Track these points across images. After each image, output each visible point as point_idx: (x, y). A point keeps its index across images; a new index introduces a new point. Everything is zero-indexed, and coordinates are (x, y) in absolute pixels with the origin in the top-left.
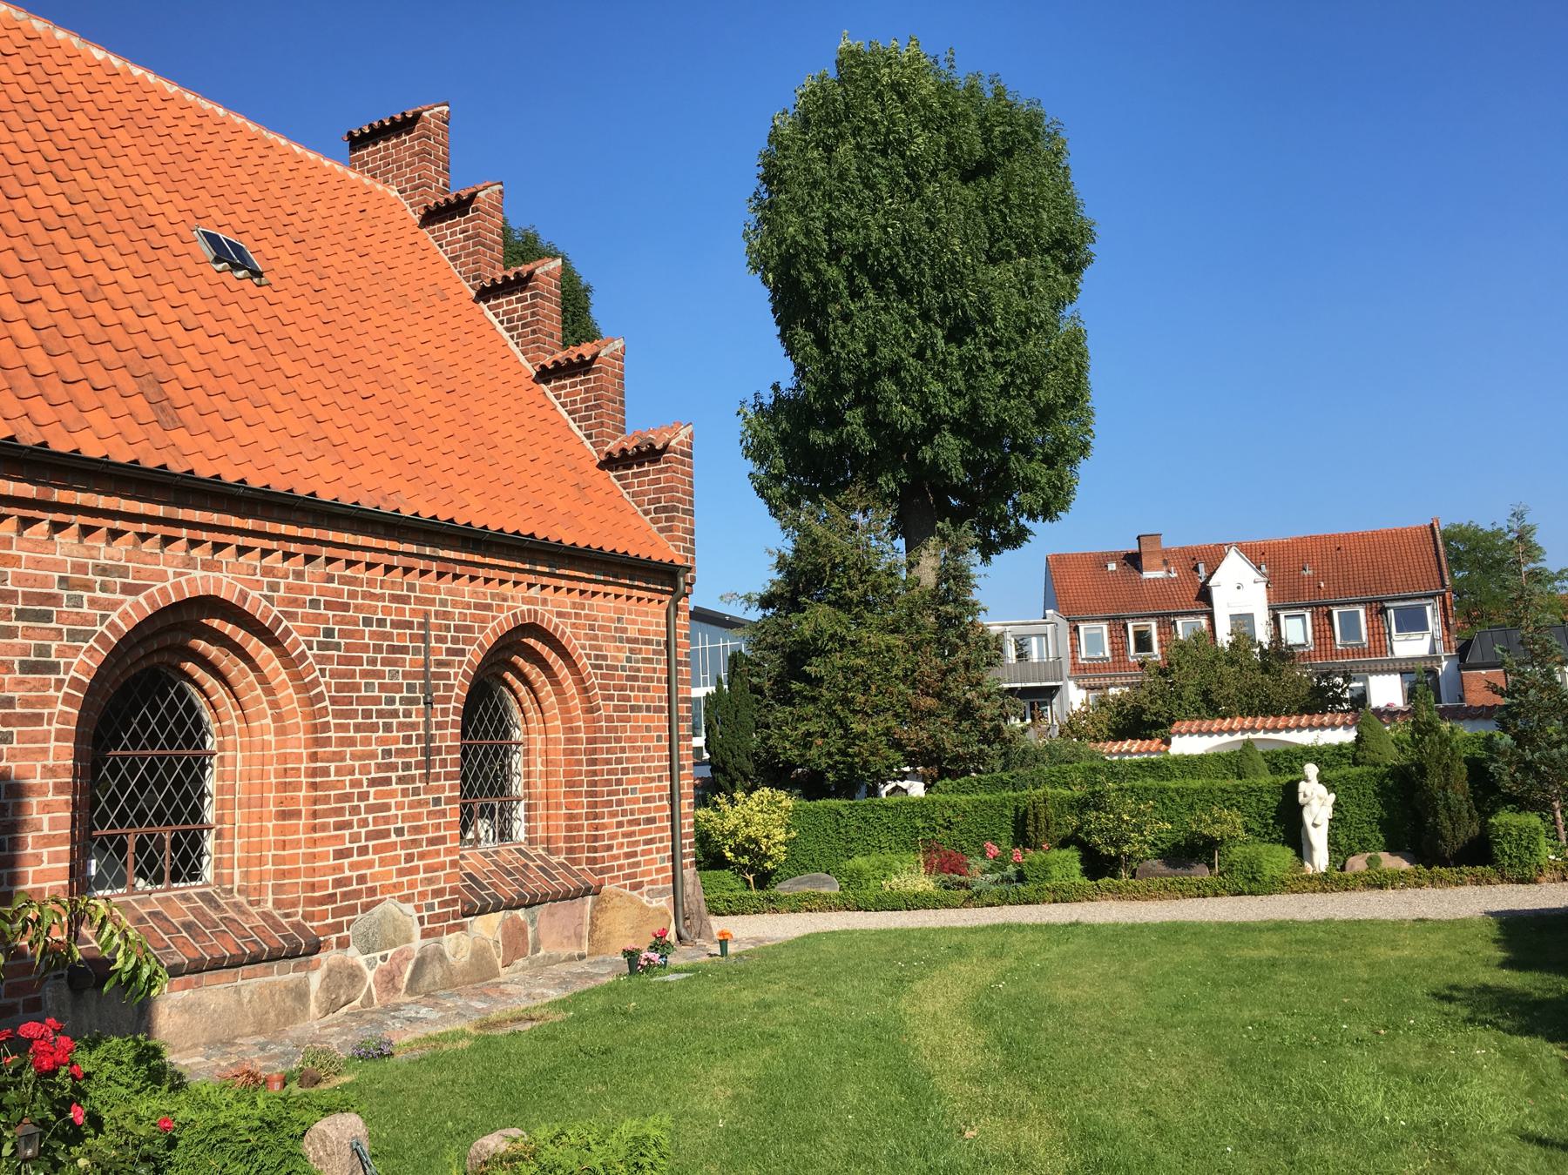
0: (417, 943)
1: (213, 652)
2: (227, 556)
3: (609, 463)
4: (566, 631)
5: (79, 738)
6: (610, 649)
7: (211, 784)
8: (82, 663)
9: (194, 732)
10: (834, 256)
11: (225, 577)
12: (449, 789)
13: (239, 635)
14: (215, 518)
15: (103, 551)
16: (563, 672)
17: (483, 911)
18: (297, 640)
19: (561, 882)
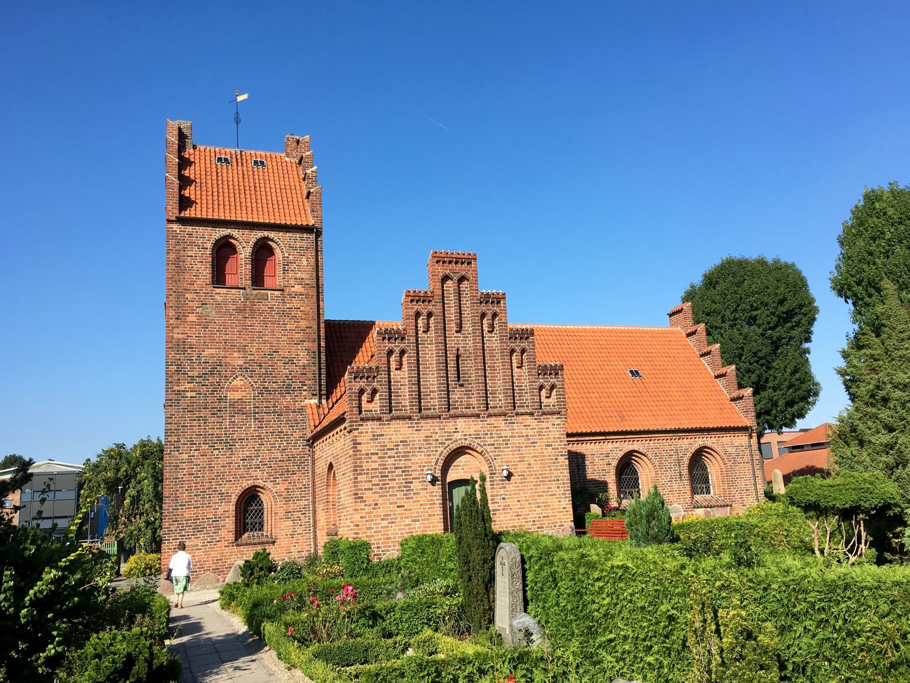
0: (683, 513)
1: (636, 459)
2: (635, 442)
3: (732, 400)
4: (715, 447)
5: (616, 475)
6: (729, 450)
7: (640, 482)
8: (615, 463)
9: (636, 473)
10: (859, 283)
11: (635, 446)
12: (687, 483)
13: (640, 455)
14: (632, 436)
15: (616, 445)
16: (717, 456)
17: (698, 508)
18: (650, 456)
19: (720, 503)
